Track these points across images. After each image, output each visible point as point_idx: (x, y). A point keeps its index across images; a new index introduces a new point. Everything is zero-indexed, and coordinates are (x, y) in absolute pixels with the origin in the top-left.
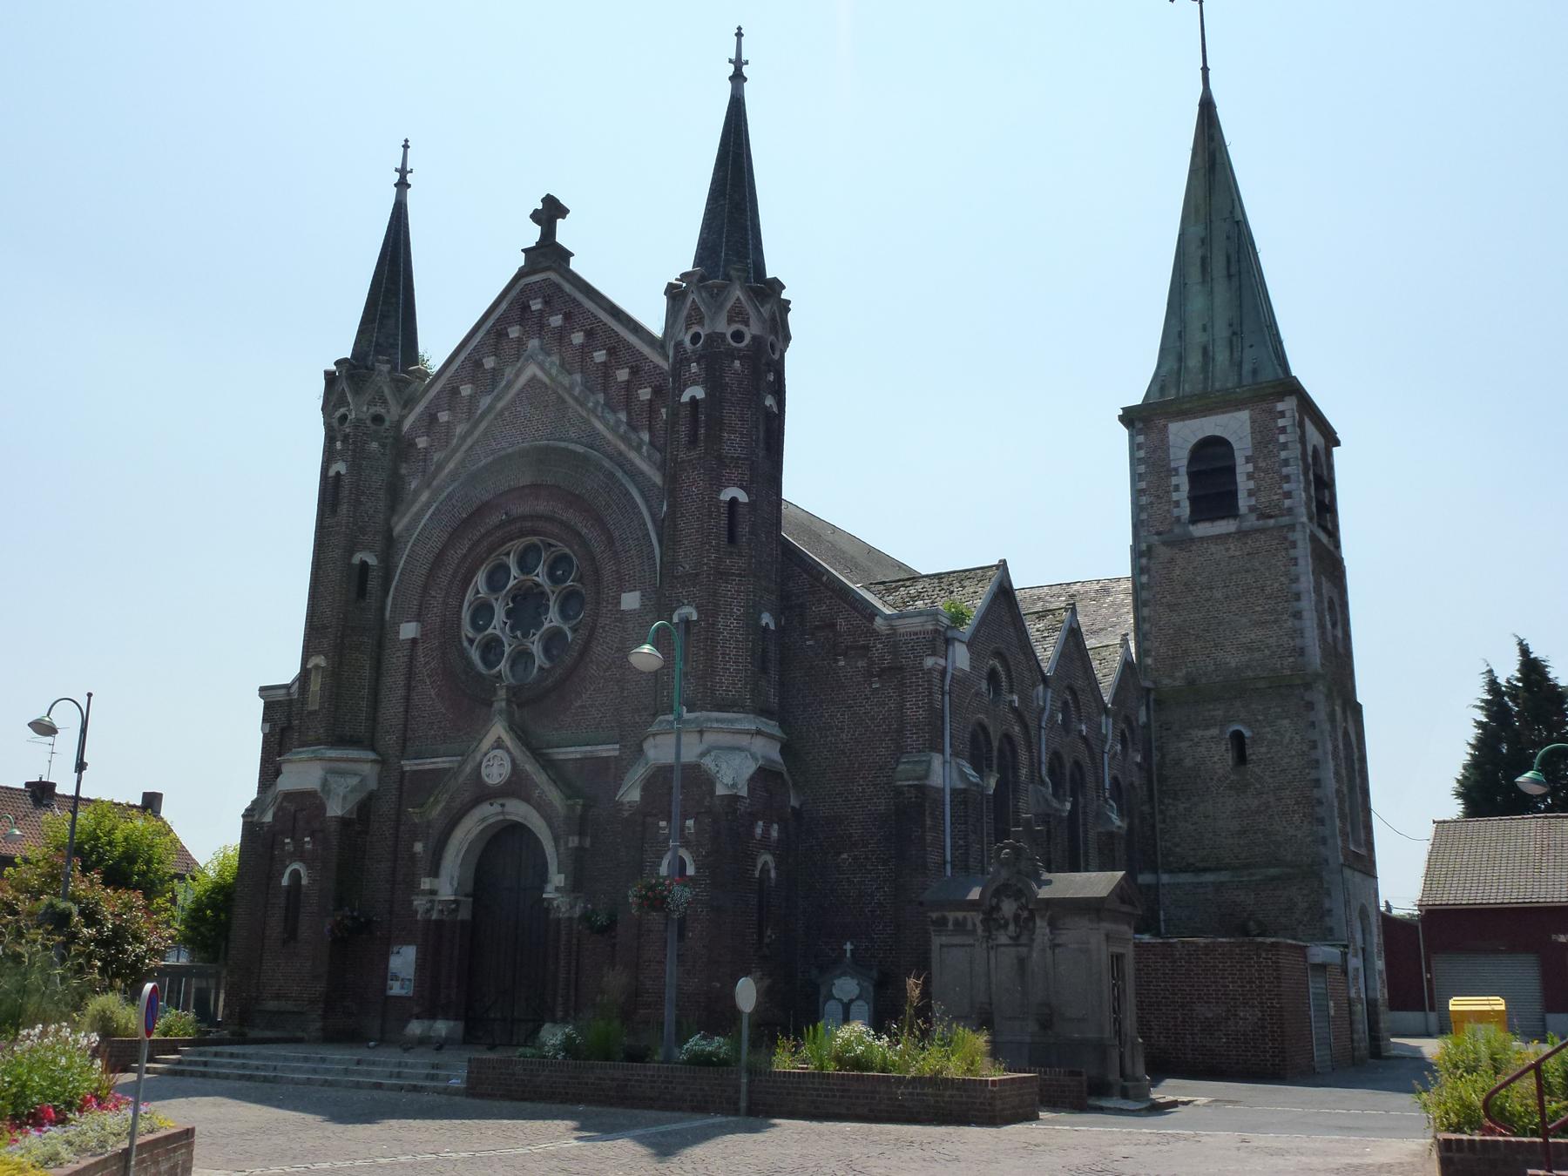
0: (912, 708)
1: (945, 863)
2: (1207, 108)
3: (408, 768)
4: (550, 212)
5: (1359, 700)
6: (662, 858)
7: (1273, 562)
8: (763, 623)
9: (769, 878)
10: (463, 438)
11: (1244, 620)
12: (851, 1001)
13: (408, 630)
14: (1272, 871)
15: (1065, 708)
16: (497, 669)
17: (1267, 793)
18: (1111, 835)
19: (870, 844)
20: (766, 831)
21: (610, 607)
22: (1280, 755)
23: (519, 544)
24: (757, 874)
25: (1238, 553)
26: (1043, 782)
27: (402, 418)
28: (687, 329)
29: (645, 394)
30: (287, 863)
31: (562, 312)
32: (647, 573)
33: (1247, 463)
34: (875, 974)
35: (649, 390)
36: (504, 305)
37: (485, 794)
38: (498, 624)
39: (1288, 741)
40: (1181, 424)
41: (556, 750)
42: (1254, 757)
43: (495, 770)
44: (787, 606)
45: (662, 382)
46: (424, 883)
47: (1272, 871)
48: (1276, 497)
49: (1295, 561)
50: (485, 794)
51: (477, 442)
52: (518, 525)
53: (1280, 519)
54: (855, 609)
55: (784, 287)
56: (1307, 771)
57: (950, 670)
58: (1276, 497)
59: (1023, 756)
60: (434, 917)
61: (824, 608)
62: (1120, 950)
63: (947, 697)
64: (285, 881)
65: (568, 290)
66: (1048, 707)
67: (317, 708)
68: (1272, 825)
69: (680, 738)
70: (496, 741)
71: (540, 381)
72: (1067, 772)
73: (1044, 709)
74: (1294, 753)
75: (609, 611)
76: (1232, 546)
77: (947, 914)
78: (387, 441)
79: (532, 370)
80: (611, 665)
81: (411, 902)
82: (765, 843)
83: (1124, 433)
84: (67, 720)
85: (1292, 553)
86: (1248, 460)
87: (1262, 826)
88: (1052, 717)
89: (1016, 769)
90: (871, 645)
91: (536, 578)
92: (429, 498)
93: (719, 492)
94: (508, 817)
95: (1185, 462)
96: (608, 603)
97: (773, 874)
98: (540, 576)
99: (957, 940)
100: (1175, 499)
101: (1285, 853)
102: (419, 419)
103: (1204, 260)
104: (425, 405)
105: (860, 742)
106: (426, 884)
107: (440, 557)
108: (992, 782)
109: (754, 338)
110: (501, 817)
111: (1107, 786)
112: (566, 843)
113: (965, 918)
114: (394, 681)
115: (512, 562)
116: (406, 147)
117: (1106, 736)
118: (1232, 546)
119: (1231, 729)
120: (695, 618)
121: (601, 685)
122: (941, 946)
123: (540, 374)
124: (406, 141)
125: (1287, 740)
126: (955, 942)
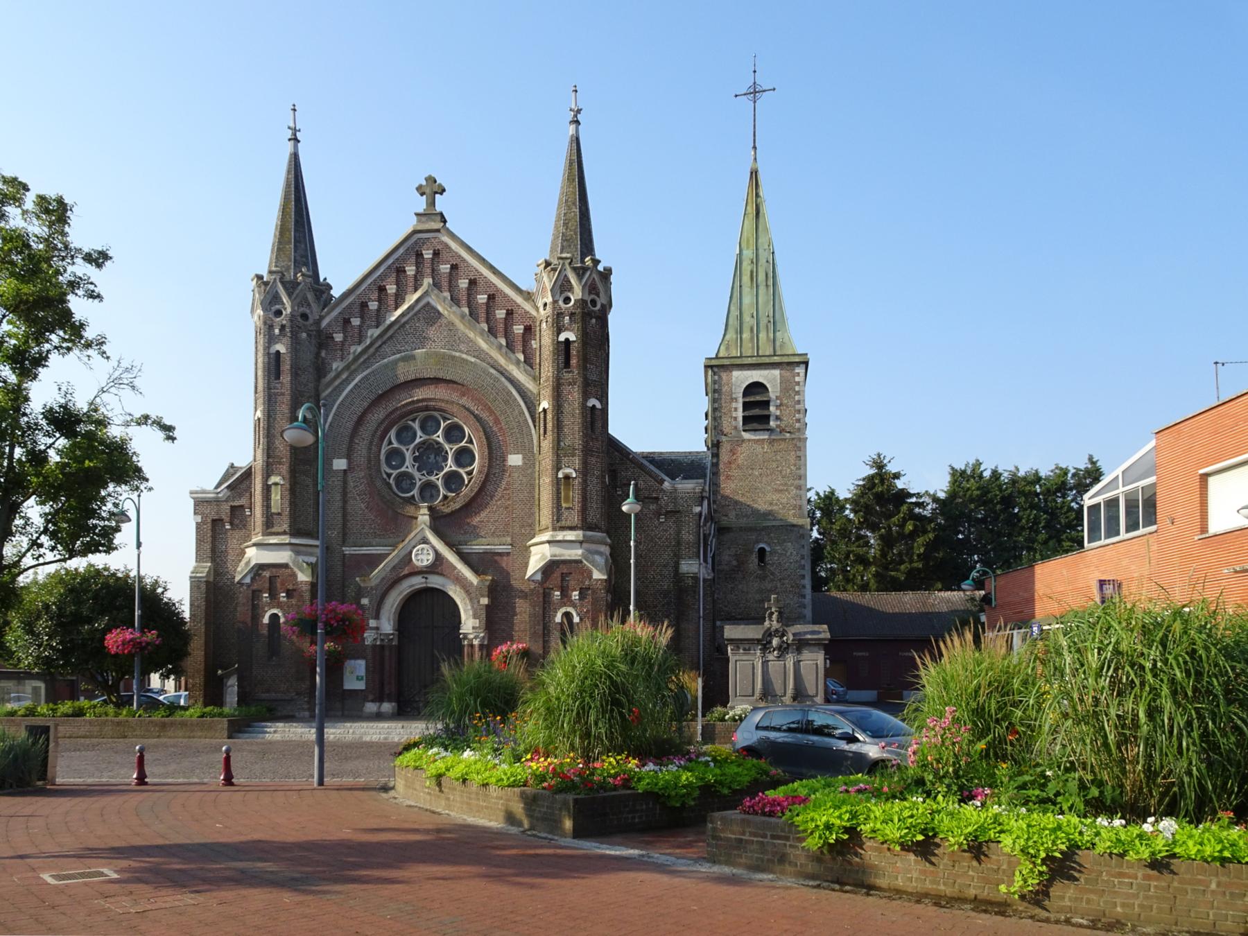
3: (347, 552)
11: (769, 488)
13: (340, 464)
16: (412, 493)
23: (422, 415)
27: (322, 318)
28: (561, 293)
30: (266, 609)
35: (522, 327)
36: (401, 251)
38: (409, 466)
40: (740, 372)
41: (465, 547)
54: (651, 476)
60: (378, 643)
64: (266, 620)
76: (766, 447)
93: (587, 401)
94: (429, 585)
98: (439, 436)
100: (734, 415)
102: (336, 319)
103: (752, 272)
104: (339, 311)
106: (372, 623)
110: (425, 585)
112: (479, 602)
115: (416, 426)
118: (766, 447)
120: (574, 475)
122: (736, 661)
125: (789, 553)
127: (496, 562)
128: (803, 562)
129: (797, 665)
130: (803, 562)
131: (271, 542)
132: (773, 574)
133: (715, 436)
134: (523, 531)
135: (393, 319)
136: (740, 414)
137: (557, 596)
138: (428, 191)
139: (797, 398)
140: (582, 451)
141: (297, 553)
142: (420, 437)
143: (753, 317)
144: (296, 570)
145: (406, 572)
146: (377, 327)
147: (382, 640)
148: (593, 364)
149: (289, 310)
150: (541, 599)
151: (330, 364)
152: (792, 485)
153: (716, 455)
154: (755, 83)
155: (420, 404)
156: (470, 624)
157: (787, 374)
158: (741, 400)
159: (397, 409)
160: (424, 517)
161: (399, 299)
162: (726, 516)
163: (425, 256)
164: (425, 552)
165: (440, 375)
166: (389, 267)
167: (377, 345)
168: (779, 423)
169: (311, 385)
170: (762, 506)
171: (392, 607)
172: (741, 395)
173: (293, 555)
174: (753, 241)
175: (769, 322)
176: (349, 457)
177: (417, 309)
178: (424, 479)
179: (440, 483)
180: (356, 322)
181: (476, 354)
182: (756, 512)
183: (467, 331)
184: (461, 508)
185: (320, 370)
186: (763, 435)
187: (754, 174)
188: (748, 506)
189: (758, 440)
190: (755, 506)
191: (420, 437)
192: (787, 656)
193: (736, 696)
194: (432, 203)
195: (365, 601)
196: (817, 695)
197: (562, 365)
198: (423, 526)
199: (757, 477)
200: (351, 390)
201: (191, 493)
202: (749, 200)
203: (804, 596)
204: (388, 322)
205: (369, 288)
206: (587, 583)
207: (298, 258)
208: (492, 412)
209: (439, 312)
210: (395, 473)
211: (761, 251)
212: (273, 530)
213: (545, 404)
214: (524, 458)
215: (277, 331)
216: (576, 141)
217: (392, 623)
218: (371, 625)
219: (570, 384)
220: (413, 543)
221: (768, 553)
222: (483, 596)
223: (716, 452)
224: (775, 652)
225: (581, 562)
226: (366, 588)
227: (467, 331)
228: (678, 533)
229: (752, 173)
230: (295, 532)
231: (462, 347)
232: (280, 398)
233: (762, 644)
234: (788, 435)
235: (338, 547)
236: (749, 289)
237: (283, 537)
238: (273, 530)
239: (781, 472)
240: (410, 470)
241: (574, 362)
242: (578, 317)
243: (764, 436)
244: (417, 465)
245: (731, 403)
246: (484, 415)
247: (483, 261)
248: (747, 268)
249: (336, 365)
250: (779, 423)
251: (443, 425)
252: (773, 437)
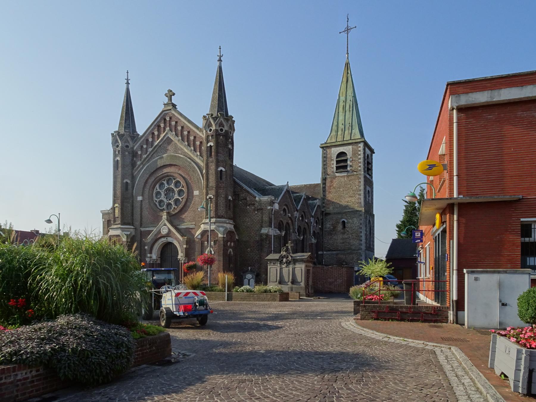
1: (272, 251)
4: (170, 94)
5: (374, 214)
8: (229, 199)
9: (231, 254)
11: (347, 196)
12: (250, 279)
13: (140, 198)
15: (302, 216)
18: (312, 244)
20: (230, 244)
23: (167, 178)
24: (228, 253)
26: (296, 233)
27: (134, 146)
28: (208, 128)
34: (255, 273)
36: (159, 119)
38: (163, 197)
40: (335, 148)
44: (236, 195)
49: (360, 182)
55: (233, 117)
57: (274, 209)
59: (291, 227)
62: (309, 269)
63: (273, 215)
66: (298, 216)
69: (161, 167)
72: (302, 230)
73: (297, 217)
76: (346, 179)
81: (146, 259)
82: (230, 247)
84: (54, 220)
85: (360, 180)
88: (299, 219)
89: (289, 230)
93: (218, 168)
97: (232, 253)
98: (172, 186)
102: (138, 146)
103: (343, 106)
106: (149, 255)
107: (146, 182)
108: (284, 233)
109: (226, 131)
111: (312, 233)
112: (183, 247)
114: (137, 211)
115: (165, 182)
117: (312, 222)
118: (346, 179)
120: (212, 197)
124: (128, 71)
125: (355, 223)
127: (190, 232)
129: (294, 270)
130: (361, 226)
131: (114, 227)
132: (348, 231)
133: (324, 176)
135: (156, 144)
136: (335, 165)
138: (168, 95)
140: (216, 188)
141: (123, 231)
142: (166, 186)
143: (343, 125)
144: (122, 237)
145: (159, 236)
146: (152, 147)
148: (221, 154)
149: (121, 145)
150: (201, 245)
151: (137, 163)
152: (357, 194)
153: (324, 184)
155: (165, 174)
156: (181, 256)
157: (355, 147)
158: (335, 160)
159: (157, 177)
160: (164, 216)
161: (159, 136)
162: (329, 208)
163: (167, 120)
164: (165, 229)
165: (172, 163)
166: (155, 125)
167: (151, 154)
168: (351, 168)
169: (130, 171)
170: (343, 203)
171: (156, 249)
172: (335, 158)
173: (121, 232)
174: (344, 93)
175: (350, 126)
176: (142, 195)
177: (165, 139)
178: (168, 202)
180: (145, 146)
181: (184, 154)
182: (341, 206)
183: (181, 146)
184: (179, 212)
185: (133, 165)
186: (345, 173)
187: (347, 65)
188: (338, 204)
189: (342, 176)
190: (341, 203)
191: (166, 186)
192: (290, 266)
193: (270, 282)
194: (170, 99)
195: (146, 247)
196: (301, 282)
197: (209, 155)
198: (164, 219)
199: (342, 192)
200: (143, 172)
201: (101, 211)
202: (344, 76)
203: (361, 241)
204: (155, 145)
205: (149, 134)
206: (216, 239)
207: (126, 126)
208: (189, 175)
209: (172, 140)
210: (158, 200)
211: (348, 97)
212: (116, 223)
213: (204, 171)
214: (199, 192)
215: (117, 153)
216: (220, 68)
219: (211, 162)
220: (161, 226)
222: (184, 245)
223: (324, 182)
224: (285, 264)
225: (214, 231)
226: (147, 243)
227: (181, 146)
228: (262, 217)
229: (346, 64)
230: (123, 223)
231: (180, 152)
232: (118, 176)
233: (280, 261)
234: (355, 173)
236: (342, 113)
237: (118, 225)
238: (116, 223)
239: (352, 188)
240: (163, 199)
241: (213, 154)
242: (214, 136)
243: (345, 174)
244: (165, 197)
245: (331, 161)
246: (186, 177)
247: (185, 118)
248: (342, 104)
249: (139, 163)
250: (351, 168)
251: (174, 182)
252: (349, 174)
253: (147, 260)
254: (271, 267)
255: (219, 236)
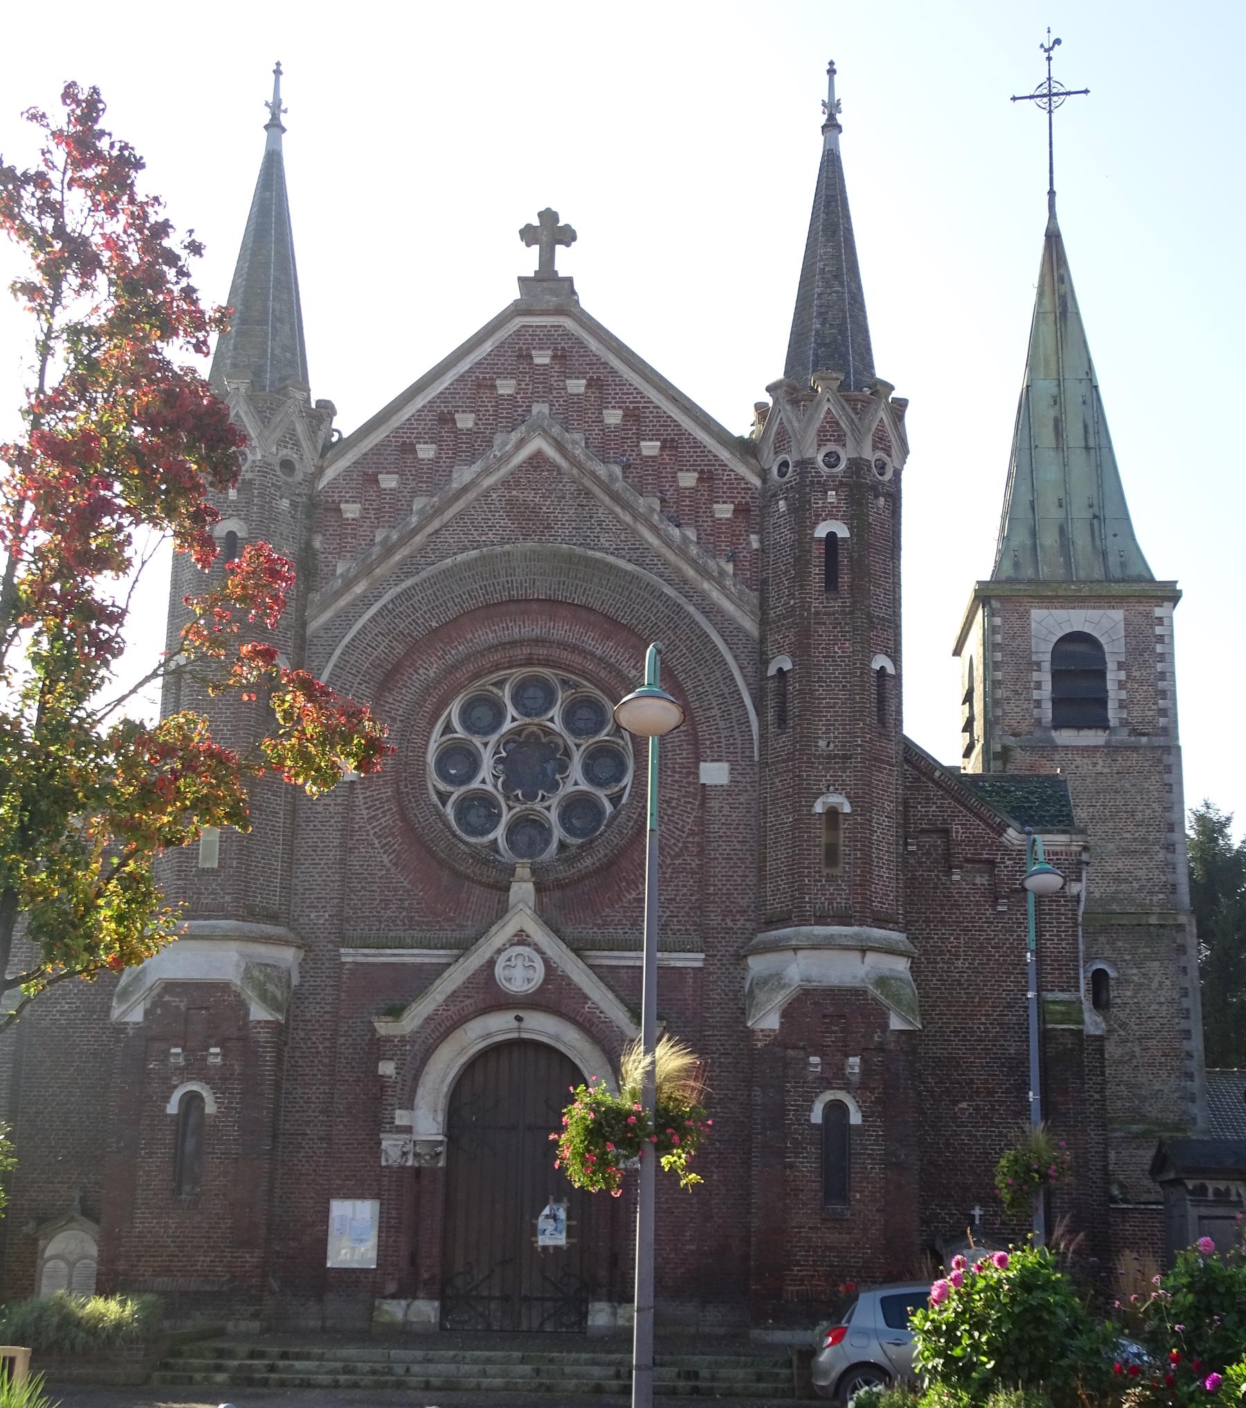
0: (1053, 940)
2: (1053, 239)
6: (813, 1102)
7: (1146, 785)
10: (427, 518)
11: (1111, 846)
14: (1135, 1128)
16: (491, 836)
17: (1132, 1042)
19: (997, 1092)
21: (677, 777)
22: (1147, 1000)
23: (518, 673)
25: (1107, 770)
27: (321, 471)
29: (724, 511)
31: (588, 376)
32: (739, 741)
33: (1119, 669)
35: (731, 507)
36: (488, 346)
37: (498, 1001)
39: (1157, 986)
40: (1045, 612)
42: (1118, 1001)
43: (518, 973)
45: (748, 499)
46: (401, 1117)
47: (1135, 1128)
48: (1151, 713)
50: (498, 1001)
51: (445, 526)
52: (526, 651)
53: (1154, 739)
56: (1177, 1020)
58: (1151, 713)
61: (934, 808)
65: (594, 349)
67: (216, 866)
68: (1137, 1077)
70: (516, 935)
71: (547, 460)
74: (1163, 1000)
75: (676, 781)
76: (1100, 762)
77: (1207, 1182)
78: (299, 500)
79: (538, 443)
80: (681, 851)
83: (1161, 574)
86: (1121, 666)
87: (1125, 1078)
90: (998, 860)
91: (549, 724)
92: (365, 591)
95: (1048, 657)
96: (675, 772)
99: (1220, 1211)
101: (1150, 1109)
103: (1057, 422)
105: (981, 973)
106: (401, 1117)
110: (515, 1035)
113: (1228, 1190)
116: (278, 72)
118: (1100, 762)
119: (1094, 968)
121: (667, 876)
123: (551, 452)
125: (1155, 985)
126: (1214, 1214)
128: (1186, 1003)
130: (1186, 1003)
134: (730, 924)
137: (816, 1065)
139: (1159, 667)
147: (416, 1155)
152: (1157, 841)
154: (1049, 79)
179: (553, 816)
195: (387, 1068)
200: (373, 618)
207: (277, 352)
210: (457, 792)
217: (440, 1118)
218: (397, 1122)
221: (1112, 982)
235: (330, 946)
253: (385, 1144)
254: (1204, 1211)
255: (892, 1027)
